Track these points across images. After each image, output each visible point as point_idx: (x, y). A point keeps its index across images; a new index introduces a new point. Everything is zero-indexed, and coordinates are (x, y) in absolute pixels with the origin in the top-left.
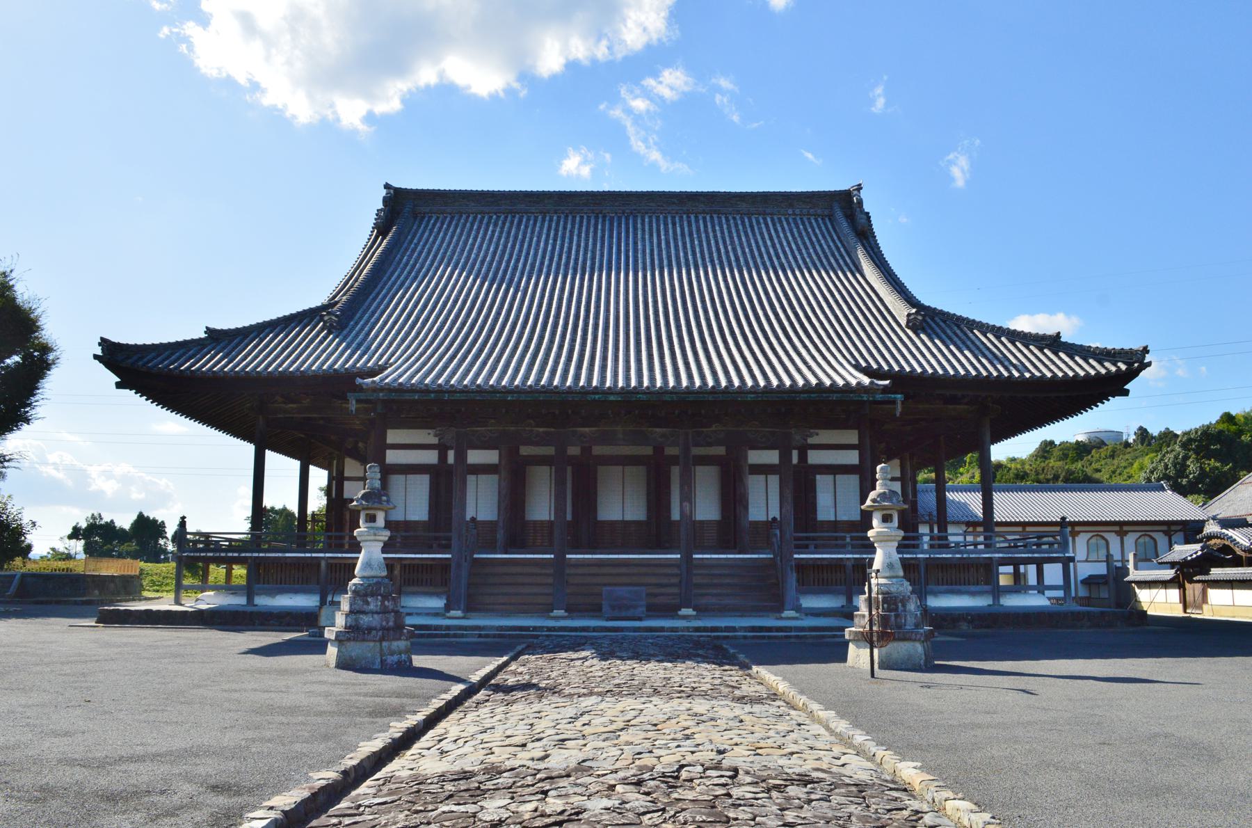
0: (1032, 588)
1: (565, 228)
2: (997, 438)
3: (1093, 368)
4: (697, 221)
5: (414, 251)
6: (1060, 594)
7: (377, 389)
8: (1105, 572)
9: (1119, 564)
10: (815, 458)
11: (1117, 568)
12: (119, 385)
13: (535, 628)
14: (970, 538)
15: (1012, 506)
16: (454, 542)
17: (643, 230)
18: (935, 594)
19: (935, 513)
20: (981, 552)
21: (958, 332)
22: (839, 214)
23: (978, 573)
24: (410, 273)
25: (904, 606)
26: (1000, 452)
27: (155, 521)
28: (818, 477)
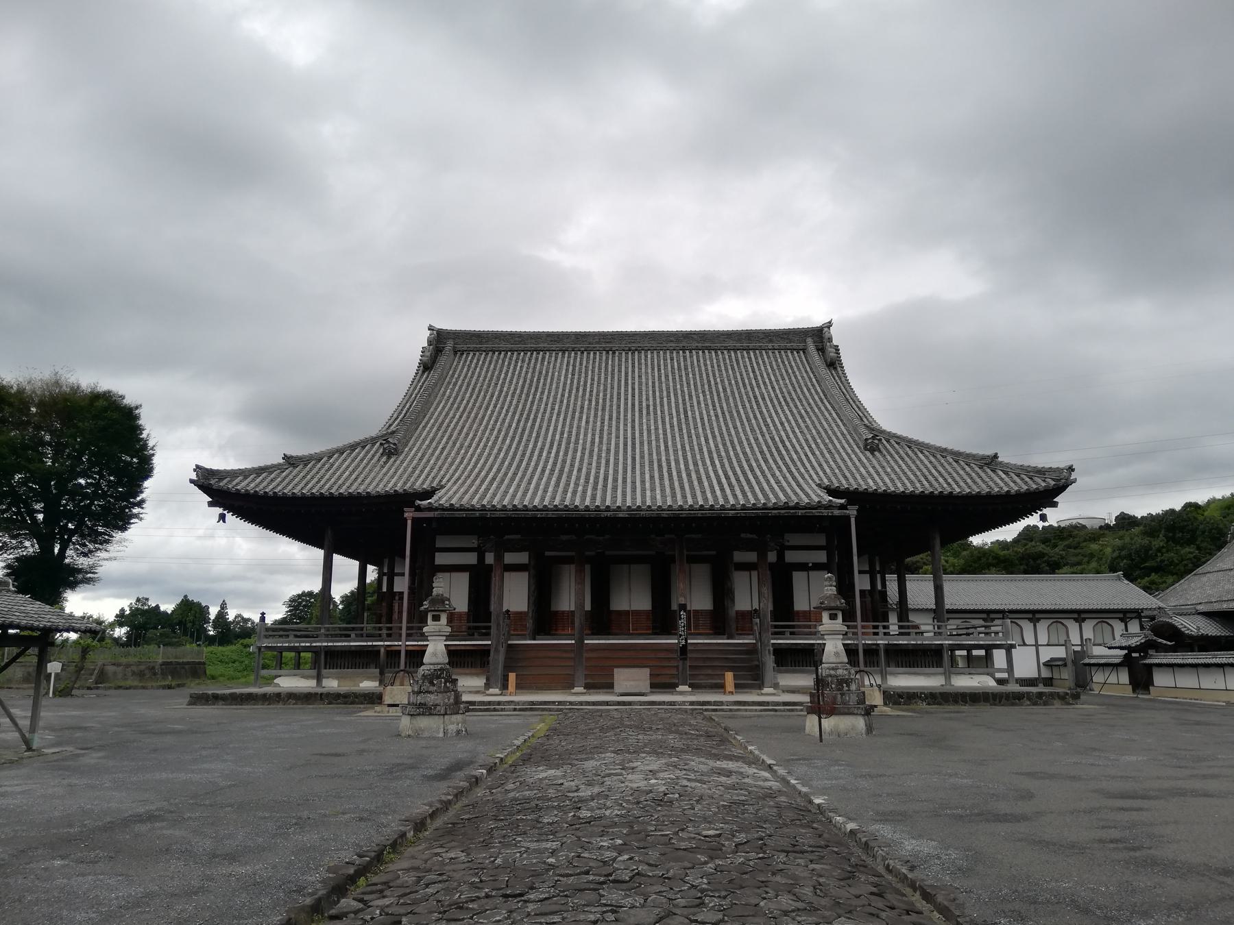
1: (581, 364)
3: (999, 484)
4: (691, 357)
5: (455, 384)
6: (1005, 675)
7: (430, 508)
8: (1063, 655)
9: (1078, 648)
10: (791, 557)
13: (560, 703)
15: (966, 592)
16: (493, 631)
17: (646, 365)
22: (811, 347)
24: (452, 404)
25: (848, 686)
27: (199, 604)
28: (795, 573)
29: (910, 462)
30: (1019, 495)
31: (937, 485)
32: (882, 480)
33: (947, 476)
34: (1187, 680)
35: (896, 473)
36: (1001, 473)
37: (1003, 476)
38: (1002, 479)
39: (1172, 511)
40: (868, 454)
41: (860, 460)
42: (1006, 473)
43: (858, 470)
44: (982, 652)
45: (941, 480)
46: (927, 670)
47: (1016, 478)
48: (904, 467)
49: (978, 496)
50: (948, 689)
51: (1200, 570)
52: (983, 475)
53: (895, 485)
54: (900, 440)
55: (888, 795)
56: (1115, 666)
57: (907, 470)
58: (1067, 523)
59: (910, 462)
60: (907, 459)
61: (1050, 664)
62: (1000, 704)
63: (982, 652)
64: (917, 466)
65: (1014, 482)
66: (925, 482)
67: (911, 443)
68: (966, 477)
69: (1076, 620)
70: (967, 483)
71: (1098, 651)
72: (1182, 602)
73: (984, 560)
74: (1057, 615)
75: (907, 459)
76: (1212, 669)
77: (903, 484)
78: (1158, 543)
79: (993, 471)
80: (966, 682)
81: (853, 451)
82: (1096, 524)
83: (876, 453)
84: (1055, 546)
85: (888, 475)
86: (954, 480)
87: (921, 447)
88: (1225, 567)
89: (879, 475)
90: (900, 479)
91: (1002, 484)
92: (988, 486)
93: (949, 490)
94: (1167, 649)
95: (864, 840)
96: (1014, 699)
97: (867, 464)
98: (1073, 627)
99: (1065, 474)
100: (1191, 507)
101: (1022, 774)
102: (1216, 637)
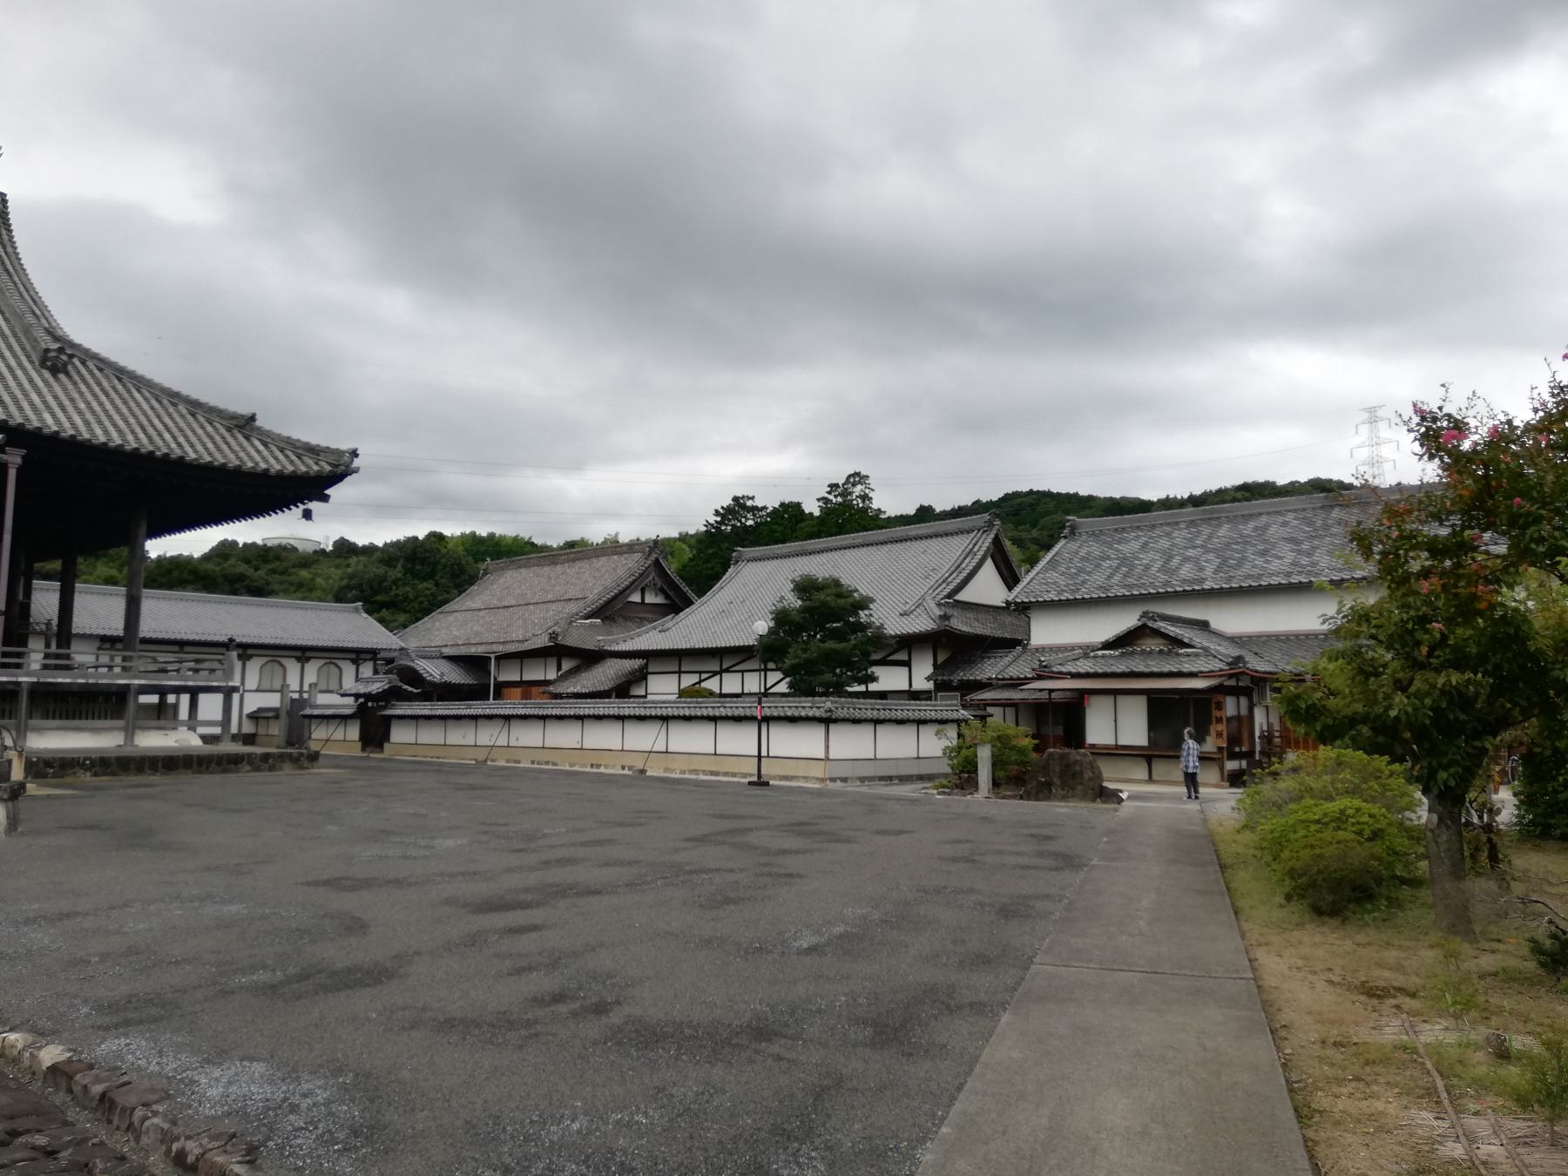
0: (183, 723)
2: (156, 533)
3: (254, 457)
6: (217, 730)
9: (296, 696)
11: (293, 700)
12: (864, 604)
14: (105, 659)
15: (167, 615)
18: (39, 730)
19: (55, 622)
20: (103, 676)
21: (119, 387)
23: (101, 703)
26: (158, 548)
29: (118, 402)
30: (280, 476)
31: (161, 443)
32: (69, 418)
33: (177, 433)
34: (431, 735)
35: (93, 412)
36: (257, 443)
37: (261, 447)
38: (258, 452)
39: (415, 539)
40: (47, 374)
41: (31, 381)
42: (265, 444)
43: (26, 395)
44: (154, 699)
45: (167, 436)
46: (89, 723)
47: (278, 453)
48: (108, 406)
49: (223, 469)
50: (128, 751)
51: (446, 608)
52: (230, 440)
53: (90, 430)
54: (103, 364)
55: (104, 957)
56: (344, 718)
57: (112, 412)
58: (276, 542)
59: (118, 402)
60: (114, 395)
61: (255, 717)
62: (208, 771)
63: (154, 699)
64: (130, 410)
65: (276, 458)
66: (141, 435)
67: (121, 373)
68: (206, 440)
69: (298, 659)
70: (207, 449)
71: (322, 699)
72: (424, 643)
73: (176, 574)
74: (275, 652)
75: (114, 395)
76: (463, 722)
77: (106, 432)
78: (396, 573)
79: (247, 438)
80: (153, 741)
81: (20, 365)
82: (310, 548)
83: (62, 376)
84: (257, 569)
85: (80, 413)
86: (188, 440)
87: (140, 382)
88: (474, 606)
89: (63, 409)
90: (100, 422)
91: (258, 458)
92: (238, 458)
93: (178, 452)
94: (410, 698)
95: (97, 1089)
96: (229, 763)
97: (45, 390)
98: (293, 668)
99: (346, 458)
100: (437, 537)
101: (316, 884)
102: (459, 685)
